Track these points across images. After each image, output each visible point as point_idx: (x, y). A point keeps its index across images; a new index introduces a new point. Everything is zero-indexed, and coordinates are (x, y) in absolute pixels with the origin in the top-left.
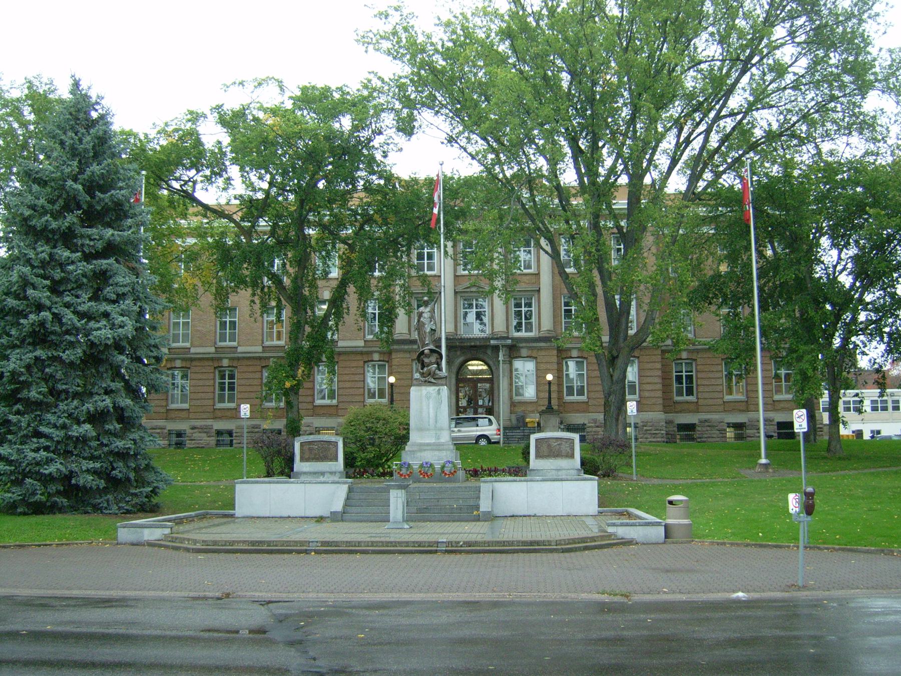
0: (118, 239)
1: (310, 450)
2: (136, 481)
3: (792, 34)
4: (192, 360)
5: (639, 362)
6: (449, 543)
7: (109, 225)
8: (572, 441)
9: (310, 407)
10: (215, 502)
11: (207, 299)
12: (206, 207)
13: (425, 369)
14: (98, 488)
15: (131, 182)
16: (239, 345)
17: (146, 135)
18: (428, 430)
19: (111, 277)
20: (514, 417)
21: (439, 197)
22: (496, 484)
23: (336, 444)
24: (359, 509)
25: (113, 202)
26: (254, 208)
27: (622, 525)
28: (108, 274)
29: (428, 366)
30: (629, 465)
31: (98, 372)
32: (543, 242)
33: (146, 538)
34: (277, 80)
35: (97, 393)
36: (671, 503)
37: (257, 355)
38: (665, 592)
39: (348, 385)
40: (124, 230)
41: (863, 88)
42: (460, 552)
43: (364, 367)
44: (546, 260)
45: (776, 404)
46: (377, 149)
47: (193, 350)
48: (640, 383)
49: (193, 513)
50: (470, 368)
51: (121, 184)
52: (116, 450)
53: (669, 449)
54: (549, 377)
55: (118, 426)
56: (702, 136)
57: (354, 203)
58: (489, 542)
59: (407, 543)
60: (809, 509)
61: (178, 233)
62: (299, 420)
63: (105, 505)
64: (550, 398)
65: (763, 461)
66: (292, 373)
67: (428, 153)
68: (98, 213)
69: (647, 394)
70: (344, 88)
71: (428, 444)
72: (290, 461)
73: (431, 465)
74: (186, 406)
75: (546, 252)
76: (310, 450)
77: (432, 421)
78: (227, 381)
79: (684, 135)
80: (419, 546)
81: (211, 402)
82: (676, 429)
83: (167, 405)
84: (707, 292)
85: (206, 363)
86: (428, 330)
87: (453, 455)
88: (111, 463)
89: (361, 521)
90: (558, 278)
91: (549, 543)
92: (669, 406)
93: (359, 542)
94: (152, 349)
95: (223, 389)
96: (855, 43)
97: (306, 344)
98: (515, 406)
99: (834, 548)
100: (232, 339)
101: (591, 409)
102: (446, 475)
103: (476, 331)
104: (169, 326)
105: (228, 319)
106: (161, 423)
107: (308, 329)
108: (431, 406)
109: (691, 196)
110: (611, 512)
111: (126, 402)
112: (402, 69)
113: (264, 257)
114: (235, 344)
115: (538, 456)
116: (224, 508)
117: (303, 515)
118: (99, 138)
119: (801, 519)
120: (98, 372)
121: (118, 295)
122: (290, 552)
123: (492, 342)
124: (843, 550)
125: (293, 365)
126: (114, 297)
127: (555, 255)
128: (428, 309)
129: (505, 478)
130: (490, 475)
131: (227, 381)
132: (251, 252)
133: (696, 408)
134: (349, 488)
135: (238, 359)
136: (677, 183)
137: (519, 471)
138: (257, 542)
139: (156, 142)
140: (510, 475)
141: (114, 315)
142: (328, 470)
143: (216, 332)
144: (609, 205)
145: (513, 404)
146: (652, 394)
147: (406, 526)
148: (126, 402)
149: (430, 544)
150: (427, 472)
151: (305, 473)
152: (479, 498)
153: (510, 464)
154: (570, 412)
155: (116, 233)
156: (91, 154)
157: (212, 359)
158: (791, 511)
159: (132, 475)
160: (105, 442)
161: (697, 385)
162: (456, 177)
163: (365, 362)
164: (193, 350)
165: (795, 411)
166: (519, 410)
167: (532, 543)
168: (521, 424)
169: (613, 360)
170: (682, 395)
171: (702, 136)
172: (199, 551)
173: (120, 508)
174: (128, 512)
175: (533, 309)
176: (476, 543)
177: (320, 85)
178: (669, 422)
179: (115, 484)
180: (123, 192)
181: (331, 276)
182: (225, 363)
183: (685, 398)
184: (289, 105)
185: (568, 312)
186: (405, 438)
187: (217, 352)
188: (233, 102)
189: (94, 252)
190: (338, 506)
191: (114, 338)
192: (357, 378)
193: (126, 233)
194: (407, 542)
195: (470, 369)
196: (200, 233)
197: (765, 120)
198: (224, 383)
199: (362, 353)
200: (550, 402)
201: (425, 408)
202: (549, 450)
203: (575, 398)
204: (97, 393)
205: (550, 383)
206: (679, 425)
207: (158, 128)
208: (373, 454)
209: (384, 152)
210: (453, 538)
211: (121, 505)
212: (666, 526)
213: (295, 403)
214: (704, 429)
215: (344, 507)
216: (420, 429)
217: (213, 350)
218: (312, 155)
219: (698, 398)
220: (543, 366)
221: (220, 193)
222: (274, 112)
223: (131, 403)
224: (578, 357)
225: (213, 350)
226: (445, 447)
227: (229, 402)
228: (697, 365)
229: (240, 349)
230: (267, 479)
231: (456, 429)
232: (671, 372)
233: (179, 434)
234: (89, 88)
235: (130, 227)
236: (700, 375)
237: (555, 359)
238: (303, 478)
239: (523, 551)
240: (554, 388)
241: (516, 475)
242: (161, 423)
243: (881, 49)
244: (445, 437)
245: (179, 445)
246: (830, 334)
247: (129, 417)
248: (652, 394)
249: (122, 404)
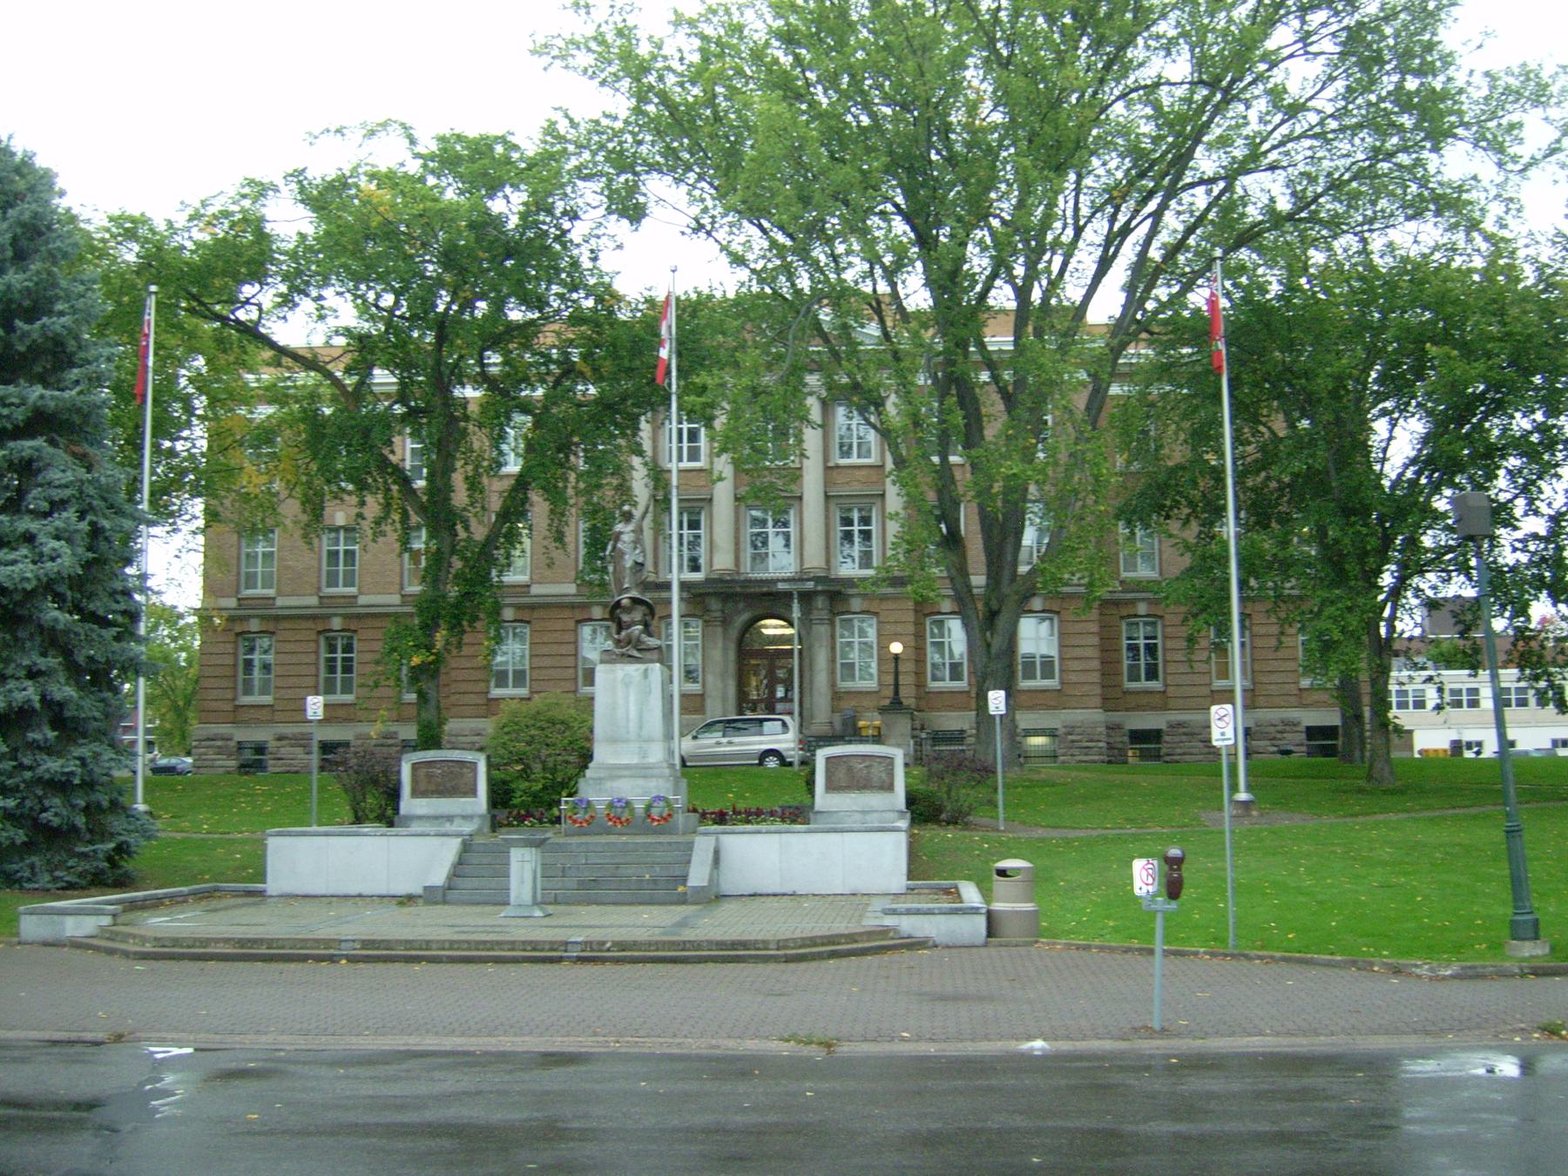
0: (52, 404)
1: (429, 776)
2: (91, 831)
3: (1305, 38)
4: (277, 618)
5: (1061, 621)
6: (588, 944)
7: (44, 381)
8: (889, 761)
10: (245, 868)
11: (291, 509)
12: (282, 351)
13: (624, 633)
14: (13, 843)
15: (80, 304)
16: (280, 593)
17: (170, 224)
18: (627, 741)
19: (39, 471)
20: (837, 719)
21: (670, 327)
22: (722, 837)
23: (473, 766)
24: (476, 882)
25: (47, 338)
26: (364, 350)
27: (909, 912)
28: (35, 465)
29: (629, 627)
30: (992, 803)
31: (16, 639)
33: (69, 933)
34: (404, 126)
35: (12, 676)
36: (1002, 873)
37: (309, 612)
38: (903, 1039)
39: (548, 662)
40: (62, 390)
41: (1438, 136)
42: (603, 960)
43: (575, 631)
45: (1305, 694)
46: (578, 246)
47: (280, 602)
48: (1062, 659)
49: (185, 889)
50: (765, 631)
51: (59, 307)
52: (47, 776)
53: (1116, 775)
54: (896, 648)
55: (51, 735)
56: (1149, 221)
57: (547, 339)
58: (657, 943)
59: (513, 945)
60: (1173, 889)
61: (248, 398)
62: (441, 724)
63: (27, 874)
64: (897, 685)
65: (1243, 796)
66: (424, 640)
67: (667, 254)
68: (23, 356)
69: (1073, 678)
70: (510, 138)
71: (627, 767)
72: (394, 795)
73: (628, 803)
74: (267, 699)
76: (429, 776)
77: (633, 726)
78: (339, 655)
79: (1122, 219)
80: (534, 949)
82: (1126, 739)
84: (1155, 500)
85: (305, 624)
86: (629, 563)
87: (670, 785)
88: (40, 799)
89: (486, 903)
91: (765, 944)
92: (1112, 698)
93: (428, 942)
94: (119, 598)
95: (332, 669)
96: (1418, 55)
97: (453, 592)
98: (840, 699)
99: (1272, 957)
100: (349, 582)
101: (1171, 703)
102: (656, 820)
103: (781, 563)
104: (239, 558)
105: (342, 548)
106: (224, 729)
107: (457, 564)
108: (632, 698)
109: (1125, 329)
110: (930, 887)
111: (64, 690)
112: (614, 104)
113: (375, 435)
114: (353, 590)
115: (831, 787)
116: (248, 880)
117: (384, 892)
118: (23, 225)
119: (1158, 907)
120: (16, 639)
121: (52, 503)
122: (303, 959)
123: (781, 586)
124: (1287, 960)
125: (429, 628)
126: (45, 506)
128: (631, 527)
129: (773, 828)
130: (748, 822)
131: (339, 655)
132: (352, 427)
133: (1162, 702)
134: (464, 843)
135: (358, 616)
136: (1107, 306)
137: (798, 815)
138: (249, 940)
139: (186, 235)
140: (783, 821)
141: (42, 539)
142: (459, 811)
143: (320, 570)
144: (981, 345)
145: (837, 696)
146: (1082, 678)
147: (538, 913)
148: (64, 690)
149: (553, 945)
150: (620, 816)
151: (420, 818)
152: (689, 862)
153: (787, 799)
154: (938, 710)
155: (48, 393)
156: (9, 253)
157: (314, 617)
158: (1137, 892)
159: (80, 821)
160: (27, 761)
161: (1165, 662)
162: (718, 294)
163: (578, 622)
164: (280, 602)
165: (1214, 708)
166: (848, 705)
167: (734, 945)
168: (850, 731)
169: (992, 615)
171: (1149, 221)
172: (145, 957)
173: (55, 879)
174: (71, 886)
175: (873, 528)
176: (634, 945)
177: (472, 133)
178: (1112, 728)
179: (50, 837)
180: (63, 320)
181: (506, 470)
182: (337, 623)
183: (1144, 684)
184: (414, 167)
186: (586, 757)
187: (321, 606)
188: (323, 167)
189: (9, 426)
190: (439, 878)
191: (39, 579)
192: (564, 649)
193: (67, 394)
194: (513, 942)
195: (750, 633)
196: (274, 395)
197: (1265, 191)
198: (334, 659)
199: (573, 606)
200: (896, 692)
201: (621, 702)
202: (848, 778)
204: (12, 676)
205: (896, 657)
206: (1308, 728)
207: (191, 211)
208: (538, 786)
209: (592, 251)
210: (595, 935)
211: (58, 873)
212: (990, 916)
213: (432, 694)
214: (1177, 739)
215: (449, 878)
216: (613, 740)
217: (314, 601)
218: (457, 260)
219: (1166, 685)
220: (889, 628)
221: (312, 325)
222: (387, 180)
223: (74, 694)
224: (1148, 616)
225: (314, 601)
226: (656, 771)
227: (952, 679)
228: (1164, 626)
229: (362, 600)
230: (354, 828)
231: (725, 740)
232: (1118, 639)
233: (260, 749)
234: (10, 138)
235: (77, 382)
236: (1169, 644)
237: (910, 616)
238: (416, 827)
239: (714, 959)
241: (793, 822)
242: (224, 729)
243: (1472, 72)
244: (656, 754)
245: (259, 766)
246: (1372, 571)
247: (73, 718)
248: (1082, 678)
249: (58, 696)
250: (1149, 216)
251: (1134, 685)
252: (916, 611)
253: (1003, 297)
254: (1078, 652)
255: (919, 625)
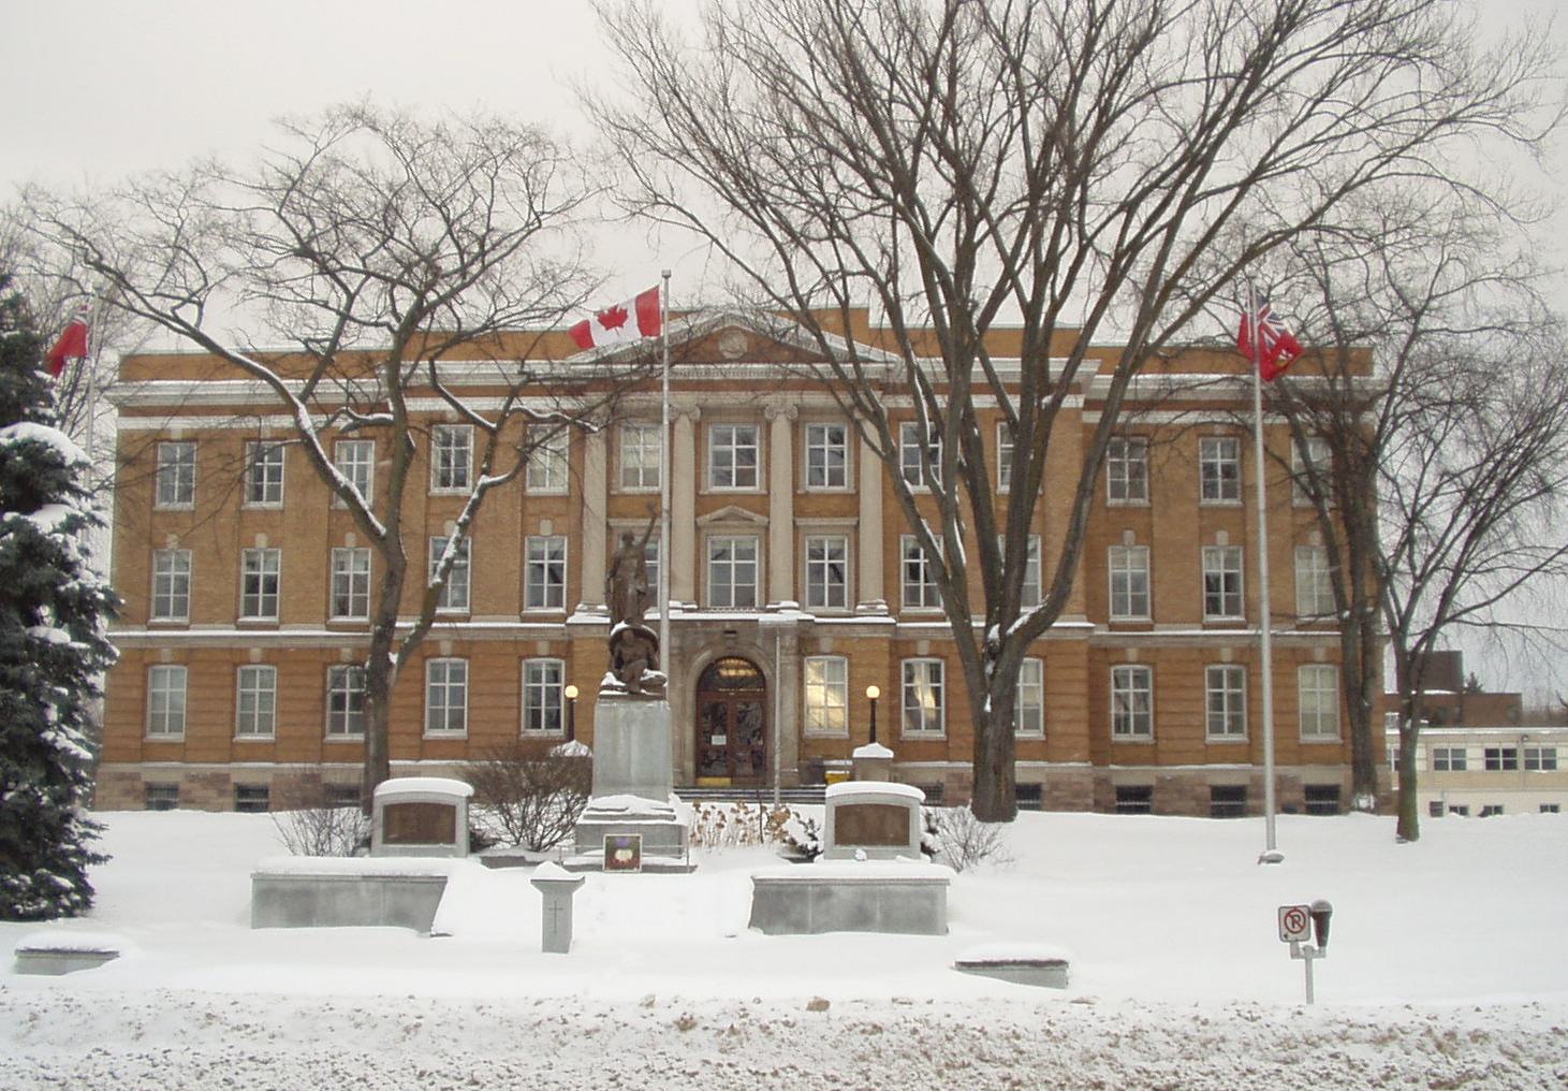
9: (415, 742)
16: (282, 622)
32: (870, 429)
44: (871, 464)
50: (724, 673)
54: (873, 692)
69: (1059, 728)
75: (874, 448)
81: (136, 732)
83: (143, 736)
90: (894, 504)
98: (807, 746)
127: (889, 456)
136: (1115, 330)
143: (238, 596)
170: (343, 731)
185: (913, 571)
203: (924, 733)
205: (873, 701)
219: (1156, 738)
240: (882, 714)
250: (1162, 228)
251: (1122, 738)
252: (891, 654)
253: (1010, 315)
254: (1064, 700)
255: (894, 669)
